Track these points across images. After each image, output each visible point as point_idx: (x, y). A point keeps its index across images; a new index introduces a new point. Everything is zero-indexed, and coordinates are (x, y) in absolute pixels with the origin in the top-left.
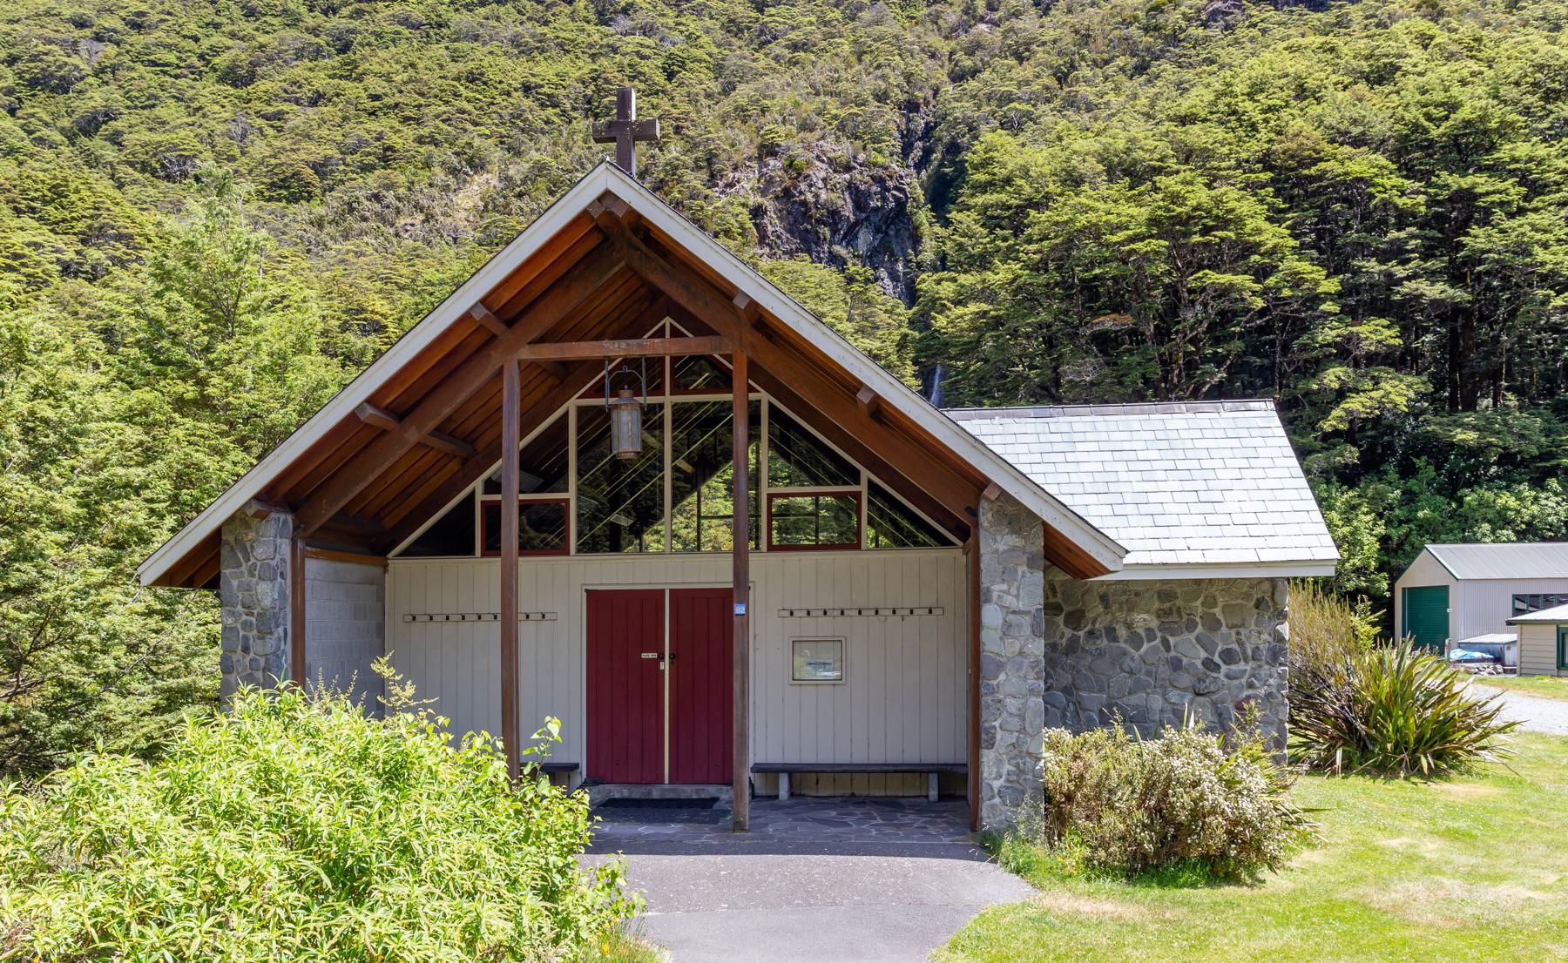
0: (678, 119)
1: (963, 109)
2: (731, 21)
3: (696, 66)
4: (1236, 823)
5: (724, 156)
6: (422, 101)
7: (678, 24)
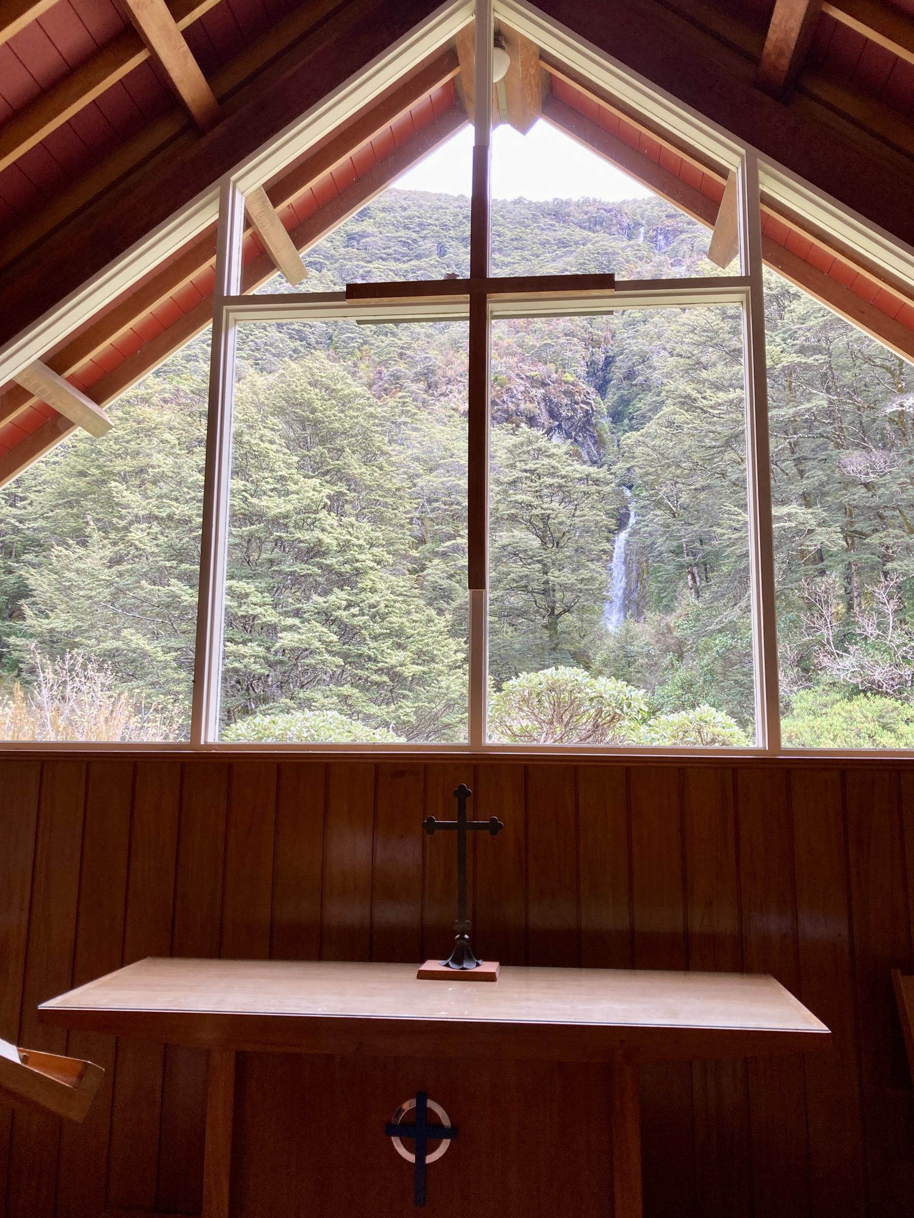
0: (402, 348)
1: (637, 345)
5: (440, 372)
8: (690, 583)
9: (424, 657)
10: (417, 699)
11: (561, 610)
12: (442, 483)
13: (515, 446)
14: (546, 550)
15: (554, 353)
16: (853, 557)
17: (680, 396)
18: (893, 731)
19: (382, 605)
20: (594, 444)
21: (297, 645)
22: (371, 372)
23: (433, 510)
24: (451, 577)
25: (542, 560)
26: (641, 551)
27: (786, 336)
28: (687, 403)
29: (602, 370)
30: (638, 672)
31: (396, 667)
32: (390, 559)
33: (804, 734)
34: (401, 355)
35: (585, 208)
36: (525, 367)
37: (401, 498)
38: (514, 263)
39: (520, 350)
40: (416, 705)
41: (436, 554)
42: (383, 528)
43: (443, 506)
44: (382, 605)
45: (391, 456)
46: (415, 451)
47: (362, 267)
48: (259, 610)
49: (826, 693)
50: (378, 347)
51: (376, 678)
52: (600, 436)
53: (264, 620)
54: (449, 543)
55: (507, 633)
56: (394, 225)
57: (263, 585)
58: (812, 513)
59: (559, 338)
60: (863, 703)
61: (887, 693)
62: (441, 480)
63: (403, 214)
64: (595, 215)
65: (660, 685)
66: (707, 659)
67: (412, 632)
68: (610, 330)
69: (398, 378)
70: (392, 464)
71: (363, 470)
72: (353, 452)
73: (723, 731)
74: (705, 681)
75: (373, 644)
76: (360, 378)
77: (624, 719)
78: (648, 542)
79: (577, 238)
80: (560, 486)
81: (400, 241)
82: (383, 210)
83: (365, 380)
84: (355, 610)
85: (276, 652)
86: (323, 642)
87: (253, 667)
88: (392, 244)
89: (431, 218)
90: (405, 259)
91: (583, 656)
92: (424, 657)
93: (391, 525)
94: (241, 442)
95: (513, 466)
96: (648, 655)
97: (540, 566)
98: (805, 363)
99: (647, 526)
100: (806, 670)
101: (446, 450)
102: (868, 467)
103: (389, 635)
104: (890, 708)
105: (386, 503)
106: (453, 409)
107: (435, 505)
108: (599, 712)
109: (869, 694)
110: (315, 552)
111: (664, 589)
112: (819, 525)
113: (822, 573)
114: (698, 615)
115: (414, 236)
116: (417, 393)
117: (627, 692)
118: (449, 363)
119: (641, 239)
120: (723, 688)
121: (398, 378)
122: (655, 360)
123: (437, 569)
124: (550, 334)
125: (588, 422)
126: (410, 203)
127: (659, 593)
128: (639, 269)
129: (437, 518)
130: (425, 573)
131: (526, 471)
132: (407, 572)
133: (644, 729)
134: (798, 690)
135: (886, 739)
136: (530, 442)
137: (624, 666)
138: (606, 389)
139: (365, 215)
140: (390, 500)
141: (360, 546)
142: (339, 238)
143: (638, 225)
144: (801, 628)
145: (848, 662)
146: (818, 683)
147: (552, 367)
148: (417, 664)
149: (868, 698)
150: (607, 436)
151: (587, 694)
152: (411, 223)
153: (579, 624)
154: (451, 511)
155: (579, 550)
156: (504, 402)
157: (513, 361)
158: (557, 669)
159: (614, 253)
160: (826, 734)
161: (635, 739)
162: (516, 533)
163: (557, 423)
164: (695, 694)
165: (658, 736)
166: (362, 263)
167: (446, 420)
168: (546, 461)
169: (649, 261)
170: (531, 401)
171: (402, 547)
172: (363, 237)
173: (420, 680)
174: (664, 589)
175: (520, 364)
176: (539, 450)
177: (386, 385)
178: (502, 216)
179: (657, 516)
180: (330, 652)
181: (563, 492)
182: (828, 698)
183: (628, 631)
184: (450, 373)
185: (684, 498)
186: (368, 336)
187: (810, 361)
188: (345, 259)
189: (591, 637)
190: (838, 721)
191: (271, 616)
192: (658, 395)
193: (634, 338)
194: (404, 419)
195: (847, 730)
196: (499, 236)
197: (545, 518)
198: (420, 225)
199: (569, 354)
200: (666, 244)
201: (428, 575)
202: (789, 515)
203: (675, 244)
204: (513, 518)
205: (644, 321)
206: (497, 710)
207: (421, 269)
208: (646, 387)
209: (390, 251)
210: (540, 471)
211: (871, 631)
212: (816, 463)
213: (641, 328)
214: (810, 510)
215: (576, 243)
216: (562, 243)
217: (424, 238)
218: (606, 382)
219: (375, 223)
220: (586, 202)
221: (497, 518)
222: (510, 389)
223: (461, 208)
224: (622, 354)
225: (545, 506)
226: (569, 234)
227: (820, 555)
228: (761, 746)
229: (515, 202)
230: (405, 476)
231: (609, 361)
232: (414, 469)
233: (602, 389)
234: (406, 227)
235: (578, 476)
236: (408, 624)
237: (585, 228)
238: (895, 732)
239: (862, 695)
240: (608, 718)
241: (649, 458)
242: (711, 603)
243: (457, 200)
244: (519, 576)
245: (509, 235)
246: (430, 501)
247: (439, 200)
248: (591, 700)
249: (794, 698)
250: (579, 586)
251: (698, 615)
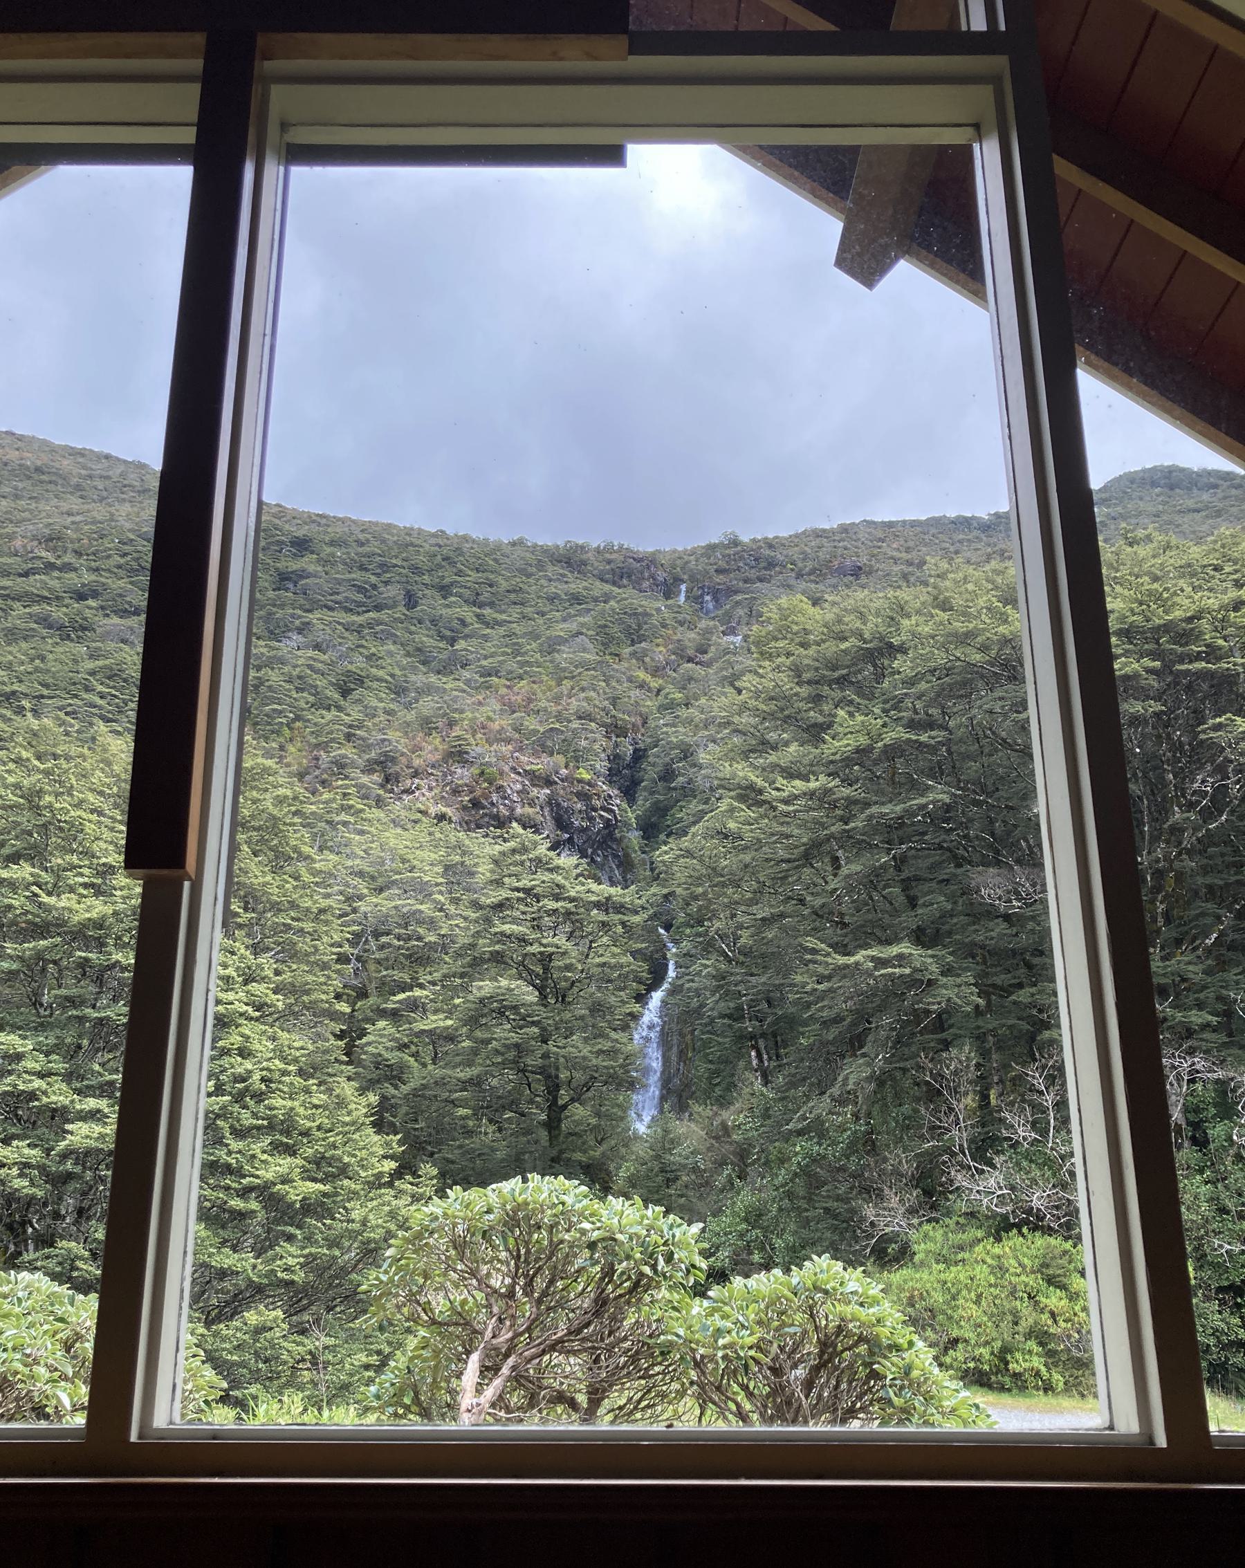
0: (350, 726)
1: (679, 735)
2: (419, 650)
3: (375, 685)
4: (1045, 1265)
5: (403, 760)
6: (45, 692)
7: (358, 646)
8: (755, 1062)
9: (326, 1167)
10: (309, 1239)
11: (567, 1098)
12: (396, 907)
13: (503, 854)
14: (545, 1006)
15: (564, 741)
16: (989, 1022)
17: (740, 787)
18: (1063, 1287)
19: (256, 1077)
20: (618, 867)
21: (93, 1143)
22: (305, 757)
23: (382, 947)
24: (403, 1047)
25: (539, 1022)
26: (684, 1017)
27: (887, 706)
28: (749, 795)
29: (629, 766)
30: (682, 1196)
31: (275, 1185)
32: (279, 1002)
33: (933, 1293)
34: (349, 737)
35: (608, 556)
36: (524, 759)
37: (327, 922)
38: (510, 622)
39: (517, 735)
40: (306, 1251)
41: (382, 1013)
42: (294, 966)
43: (396, 942)
44: (256, 1077)
45: (314, 861)
46: (357, 862)
47: (300, 617)
49: (961, 1227)
50: (315, 724)
51: (236, 1203)
52: (627, 855)
53: (45, 1100)
54: (401, 996)
55: (486, 1134)
56: (346, 564)
57: (52, 1041)
58: (932, 956)
59: (570, 721)
60: (1018, 1244)
61: (1050, 1228)
62: (393, 904)
63: (360, 550)
64: (621, 565)
65: (714, 1216)
66: (782, 1175)
67: (308, 1124)
68: (641, 715)
69: (342, 766)
70: (315, 873)
71: (268, 878)
72: (255, 854)
73: (862, 1313)
74: (780, 1209)
75: (235, 1145)
76: (288, 765)
77: (658, 1287)
78: (695, 1003)
79: (596, 593)
80: (568, 913)
81: (354, 586)
82: (332, 543)
83: (294, 768)
85: (64, 1156)
87: (18, 1183)
88: (342, 589)
89: (396, 557)
90: (360, 609)
91: (600, 1170)
92: (326, 1167)
93: (308, 963)
94: (38, 807)
95: (498, 883)
96: (695, 1169)
97: (536, 1030)
98: (916, 741)
99: (693, 981)
100: (928, 1193)
101: (404, 861)
102: (1009, 892)
103: (271, 1127)
104: (1057, 1252)
105: (302, 930)
106: (420, 812)
107: (384, 939)
108: (609, 1272)
109: (1025, 1230)
111: (717, 1073)
112: (943, 974)
113: (946, 1045)
114: (767, 1109)
115: (373, 579)
116: (369, 788)
117: (665, 1230)
118: (416, 749)
119: (682, 598)
120: (808, 1221)
121: (342, 766)
122: (703, 757)
123: (381, 1036)
124: (559, 717)
125: (611, 834)
126: (369, 536)
127: (710, 1079)
128: (679, 636)
129: (387, 959)
130: (364, 1040)
131: (518, 890)
132: (331, 1037)
133: (698, 1307)
134: (920, 1224)
135: (1054, 1300)
137: (662, 1185)
138: (635, 792)
139: (306, 549)
140: (308, 926)
142: (268, 577)
143: (678, 580)
144: (921, 1127)
145: (993, 1180)
146: (948, 1214)
147: (560, 759)
148: (314, 1180)
149: (1023, 1235)
150: (637, 856)
151: (583, 1232)
152: (370, 562)
153: (593, 1121)
154: (408, 949)
155: (597, 1009)
156: (493, 804)
157: (506, 749)
158: (525, 1180)
159: (646, 614)
160: (964, 1292)
161: (681, 1332)
162: (504, 983)
163: (567, 836)
164: (765, 1230)
165: (728, 1324)
166: (299, 612)
167: (409, 826)
168: (547, 877)
169: (691, 626)
170: (532, 804)
171: (324, 997)
172: (302, 577)
173: (310, 1208)
174: (717, 1073)
175: (517, 754)
177: (325, 776)
178: (496, 560)
179: (706, 966)
181: (572, 919)
182: (964, 1237)
183: (666, 1131)
184: (417, 762)
185: (745, 939)
186: (303, 710)
187: (924, 738)
188: (274, 606)
189: (613, 1142)
190: (981, 1272)
191: (59, 1095)
192: (706, 803)
193: (674, 725)
194: (343, 817)
195: (996, 1286)
196: (491, 586)
197: (546, 959)
198: (382, 565)
199: (583, 743)
200: (716, 608)
201: (369, 1044)
202: (900, 957)
203: (728, 607)
204: (498, 958)
205: (686, 705)
206: (399, 1269)
207: (381, 624)
208: (689, 792)
209: (339, 598)
210: (538, 890)
211: (1024, 1132)
212: (934, 884)
213: (683, 713)
214: (930, 952)
215: (596, 600)
216: (576, 599)
217: (386, 583)
218: (635, 783)
219: (318, 560)
220: (609, 549)
221: (475, 958)
222: (501, 787)
223: (440, 546)
224: (656, 746)
225: (544, 941)
226: (586, 588)
227: (941, 1022)
228: (1128, 1424)
229: (514, 544)
230: (341, 897)
231: (639, 755)
232: (355, 887)
233: (629, 793)
234: (362, 568)
235: (594, 898)
236: (301, 1111)
237: (607, 582)
238: (1066, 1289)
239: (1015, 1231)
240: (627, 1284)
241: (696, 874)
242: (787, 1091)
243: (434, 535)
244: (505, 1046)
245: (504, 585)
246: (377, 935)
247: (410, 535)
248: (592, 1246)
249: (914, 1235)
250: (594, 1062)
251: (767, 1109)
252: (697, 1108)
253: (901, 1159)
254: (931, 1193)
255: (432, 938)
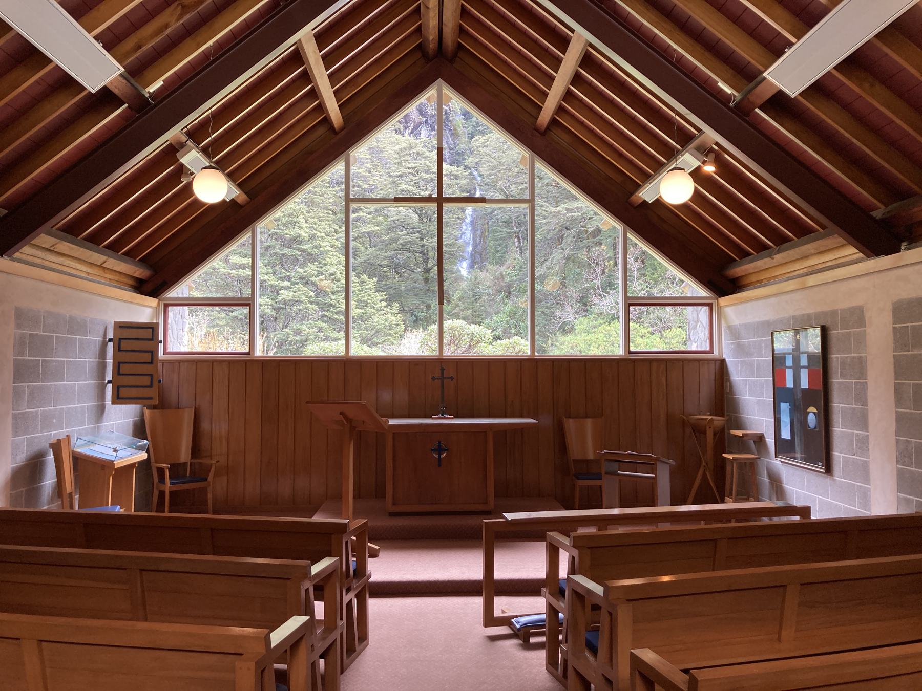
10: (359, 329)
13: (401, 150)
48: (267, 277)
52: (455, 129)
84: (322, 277)
86: (307, 297)
87: (266, 311)
100: (585, 305)
108: (472, 340)
110: (296, 240)
111: (500, 245)
133: (490, 347)
136: (411, 148)
141: (322, 237)
146: (591, 313)
176: (418, 153)
180: (309, 302)
190: (601, 336)
202: (577, 208)
249: (576, 322)
252: (490, 267)
253: (573, 292)
254: (584, 304)
255: (366, 186)
